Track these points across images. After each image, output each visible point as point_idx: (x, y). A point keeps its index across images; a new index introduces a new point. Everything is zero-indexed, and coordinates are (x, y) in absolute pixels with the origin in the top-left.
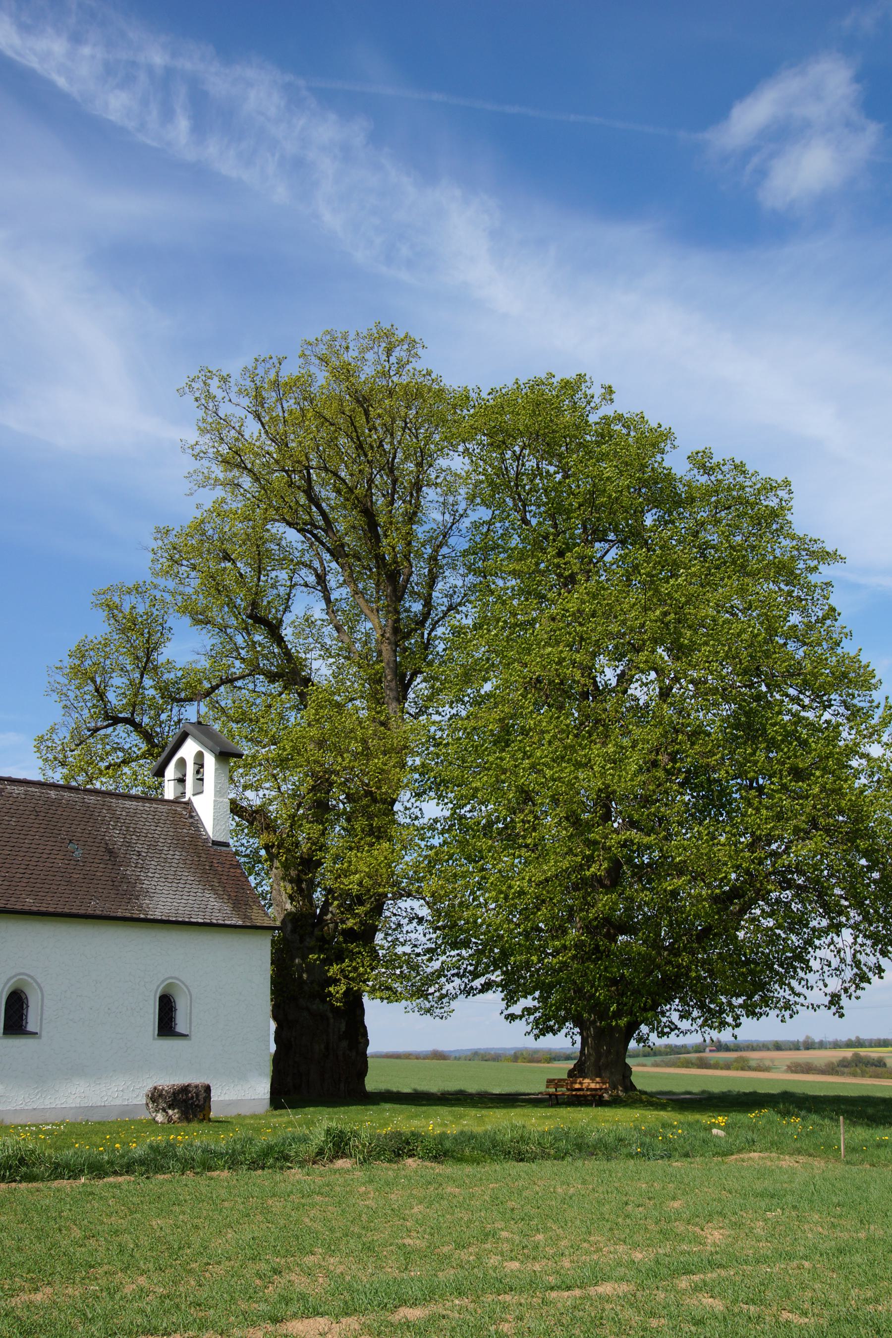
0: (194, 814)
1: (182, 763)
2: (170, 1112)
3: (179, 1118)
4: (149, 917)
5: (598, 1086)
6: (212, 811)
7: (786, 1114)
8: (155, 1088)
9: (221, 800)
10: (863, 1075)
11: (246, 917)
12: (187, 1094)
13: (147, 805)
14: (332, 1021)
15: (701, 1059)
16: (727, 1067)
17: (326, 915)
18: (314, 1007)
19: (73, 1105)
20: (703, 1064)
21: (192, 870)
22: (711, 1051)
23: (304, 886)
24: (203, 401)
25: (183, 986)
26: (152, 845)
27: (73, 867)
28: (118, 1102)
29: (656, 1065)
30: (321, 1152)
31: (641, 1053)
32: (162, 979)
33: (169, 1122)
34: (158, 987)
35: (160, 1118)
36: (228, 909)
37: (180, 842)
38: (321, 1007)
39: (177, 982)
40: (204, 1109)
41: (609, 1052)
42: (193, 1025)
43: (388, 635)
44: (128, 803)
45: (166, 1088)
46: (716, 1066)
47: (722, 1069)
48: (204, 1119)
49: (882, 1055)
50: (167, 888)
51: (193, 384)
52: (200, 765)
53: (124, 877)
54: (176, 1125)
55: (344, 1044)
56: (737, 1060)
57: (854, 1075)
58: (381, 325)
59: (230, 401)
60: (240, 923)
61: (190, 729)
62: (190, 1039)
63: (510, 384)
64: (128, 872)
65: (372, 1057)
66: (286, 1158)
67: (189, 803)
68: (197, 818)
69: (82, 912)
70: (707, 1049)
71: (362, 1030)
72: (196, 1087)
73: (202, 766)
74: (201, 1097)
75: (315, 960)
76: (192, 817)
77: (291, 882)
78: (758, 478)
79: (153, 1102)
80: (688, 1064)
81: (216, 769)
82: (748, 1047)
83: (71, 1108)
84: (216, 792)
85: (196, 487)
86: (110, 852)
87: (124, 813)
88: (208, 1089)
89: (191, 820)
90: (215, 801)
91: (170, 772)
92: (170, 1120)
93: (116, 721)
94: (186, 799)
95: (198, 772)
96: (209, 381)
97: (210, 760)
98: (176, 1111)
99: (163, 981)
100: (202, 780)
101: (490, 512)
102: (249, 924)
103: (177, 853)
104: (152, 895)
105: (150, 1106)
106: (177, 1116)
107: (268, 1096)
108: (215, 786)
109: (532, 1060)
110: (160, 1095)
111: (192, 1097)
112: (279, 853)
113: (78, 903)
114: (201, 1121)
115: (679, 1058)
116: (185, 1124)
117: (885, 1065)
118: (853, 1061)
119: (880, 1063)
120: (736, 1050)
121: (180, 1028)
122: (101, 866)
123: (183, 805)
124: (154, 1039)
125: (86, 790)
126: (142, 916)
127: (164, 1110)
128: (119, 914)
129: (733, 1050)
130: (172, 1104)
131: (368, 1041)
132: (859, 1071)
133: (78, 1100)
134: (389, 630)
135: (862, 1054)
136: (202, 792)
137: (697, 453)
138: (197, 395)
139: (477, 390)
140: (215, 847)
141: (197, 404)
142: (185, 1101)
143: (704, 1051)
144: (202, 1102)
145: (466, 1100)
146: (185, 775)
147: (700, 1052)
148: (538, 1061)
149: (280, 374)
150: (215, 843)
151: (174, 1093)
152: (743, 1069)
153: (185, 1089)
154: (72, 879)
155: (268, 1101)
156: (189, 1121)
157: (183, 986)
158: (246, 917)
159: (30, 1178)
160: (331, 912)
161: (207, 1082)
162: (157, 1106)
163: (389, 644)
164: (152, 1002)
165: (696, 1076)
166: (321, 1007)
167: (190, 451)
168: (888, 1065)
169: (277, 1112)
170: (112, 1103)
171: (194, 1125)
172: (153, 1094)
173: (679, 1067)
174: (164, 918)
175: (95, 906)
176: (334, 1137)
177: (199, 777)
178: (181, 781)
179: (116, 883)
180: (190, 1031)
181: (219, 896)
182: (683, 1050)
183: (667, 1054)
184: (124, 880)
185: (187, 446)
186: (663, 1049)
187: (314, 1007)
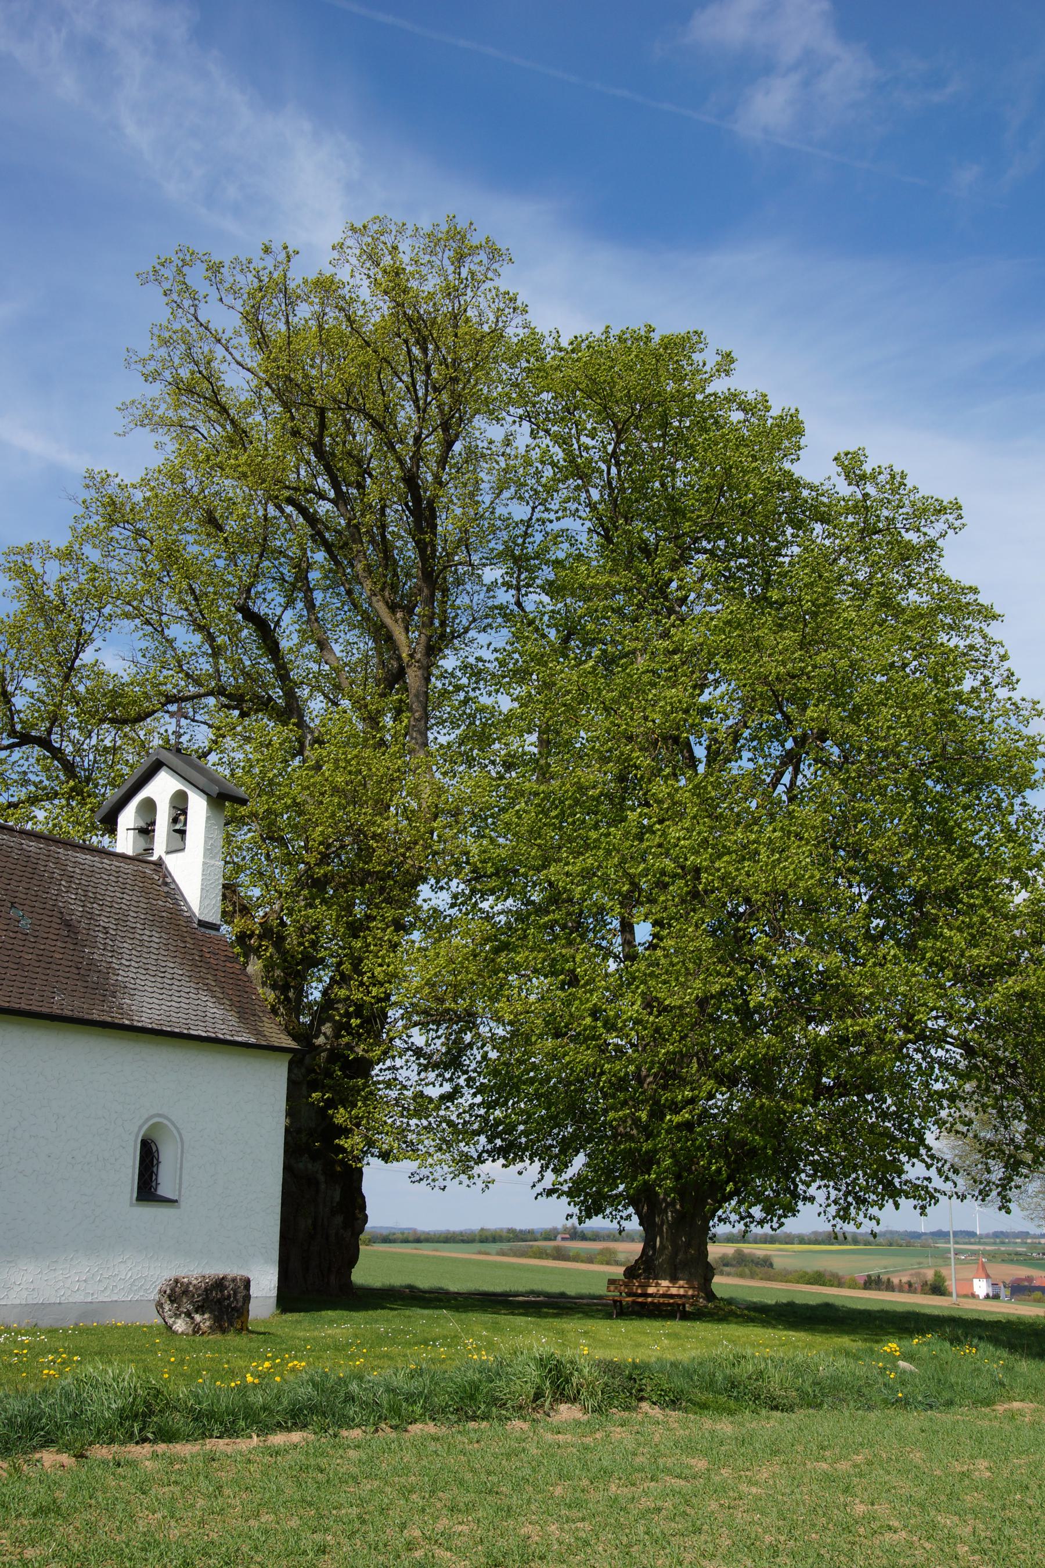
0: (168, 880)
1: (149, 806)
2: (198, 1318)
3: (210, 1327)
4: (135, 1023)
5: (682, 1292)
6: (200, 878)
7: (955, 1341)
8: (177, 1281)
9: (212, 862)
10: (752, 1276)
11: (259, 1033)
12: (222, 1291)
13: (105, 861)
14: (323, 1186)
15: (558, 1249)
16: (590, 1260)
17: (317, 1037)
18: (301, 1165)
19: (17, 1302)
20: (560, 1255)
21: (177, 959)
22: (563, 1239)
23: (291, 994)
24: (175, 296)
25: (173, 1129)
26: (122, 921)
27: (21, 943)
28: (79, 1298)
29: (502, 1253)
30: (538, 1395)
31: (477, 1238)
32: (146, 1116)
33: (195, 1332)
34: (140, 1127)
35: (180, 1325)
36: (233, 1019)
37: (156, 918)
38: (310, 1166)
39: (165, 1122)
40: (242, 1314)
41: (688, 1245)
42: (184, 1186)
43: (418, 656)
44: (81, 857)
45: (195, 1282)
46: (576, 1259)
47: (582, 1261)
48: (242, 1329)
49: (769, 1253)
50: (150, 984)
51: (163, 271)
52: (180, 807)
53: (92, 963)
54: (205, 1338)
55: (339, 1219)
56: (602, 1252)
57: (741, 1276)
58: (456, 220)
59: (221, 300)
60: (253, 1040)
61: (166, 756)
62: (179, 1207)
63: (598, 332)
64: (95, 956)
65: (374, 1239)
66: (495, 1401)
67: (159, 864)
68: (173, 886)
69: (45, 1010)
70: (559, 1237)
71: (359, 1200)
72: (234, 1280)
73: (184, 812)
74: (239, 1296)
75: (319, 1101)
76: (166, 884)
77: (274, 987)
78: (917, 496)
79: (172, 1302)
80: (541, 1254)
81: (208, 818)
82: (609, 1236)
83: (14, 1306)
84: (206, 850)
85: (132, 426)
86: (68, 924)
87: (78, 871)
88: (247, 1283)
89: (166, 889)
90: (204, 863)
91: (128, 818)
92: (196, 1330)
93: (25, 739)
94: (154, 858)
95: (175, 820)
96: (185, 270)
97: (198, 806)
98: (206, 1316)
99: (147, 1120)
100: (182, 832)
101: (529, 509)
102: (264, 1043)
103: (154, 933)
104: (132, 992)
105: (167, 1307)
106: (208, 1323)
107: (274, 1293)
108: (206, 842)
109: (406, 1241)
110: (185, 1292)
111: (229, 1296)
112: (261, 946)
113: (36, 997)
114: (240, 1331)
115: (531, 1247)
116: (218, 1336)
117: (771, 1265)
118: (734, 1258)
119: (766, 1263)
120: (594, 1240)
121: (165, 1189)
122: (59, 944)
123: (153, 867)
124: (132, 1205)
125: (23, 832)
126: (127, 1022)
127: (188, 1314)
128: (95, 1017)
129: (590, 1240)
130: (202, 1306)
131: (366, 1216)
132: (747, 1270)
133: (25, 1294)
134: (421, 649)
135: (746, 1251)
136: (183, 849)
137: (846, 454)
138: (167, 286)
139: (554, 335)
140: (203, 930)
141: (166, 299)
142: (219, 1302)
143: (555, 1239)
144: (240, 1304)
145: (449, 1301)
146: (153, 823)
147: (550, 1240)
148: (393, 1241)
149: (289, 275)
150: (202, 924)
151: (206, 1290)
152: (608, 1263)
153: (220, 1284)
154: (22, 960)
155: (273, 1301)
156: (224, 1331)
157: (173, 1129)
158: (259, 1033)
159: (167, 1436)
160: (325, 1034)
161: (245, 1273)
162: (178, 1308)
163: (419, 668)
164: (131, 1150)
165: (584, 1273)
166: (310, 1166)
167: (140, 367)
168: (775, 1266)
169: (289, 1316)
170: (71, 1300)
171: (232, 1339)
172: (173, 1290)
173: (530, 1257)
174: (156, 1027)
175: (60, 1003)
176: (550, 1371)
177: (178, 827)
178: (146, 831)
179: (82, 972)
180: (180, 1195)
181: (219, 1001)
182: (529, 1237)
183: (509, 1241)
184: (93, 968)
185: (135, 359)
186: (505, 1234)
187: (301, 1165)
